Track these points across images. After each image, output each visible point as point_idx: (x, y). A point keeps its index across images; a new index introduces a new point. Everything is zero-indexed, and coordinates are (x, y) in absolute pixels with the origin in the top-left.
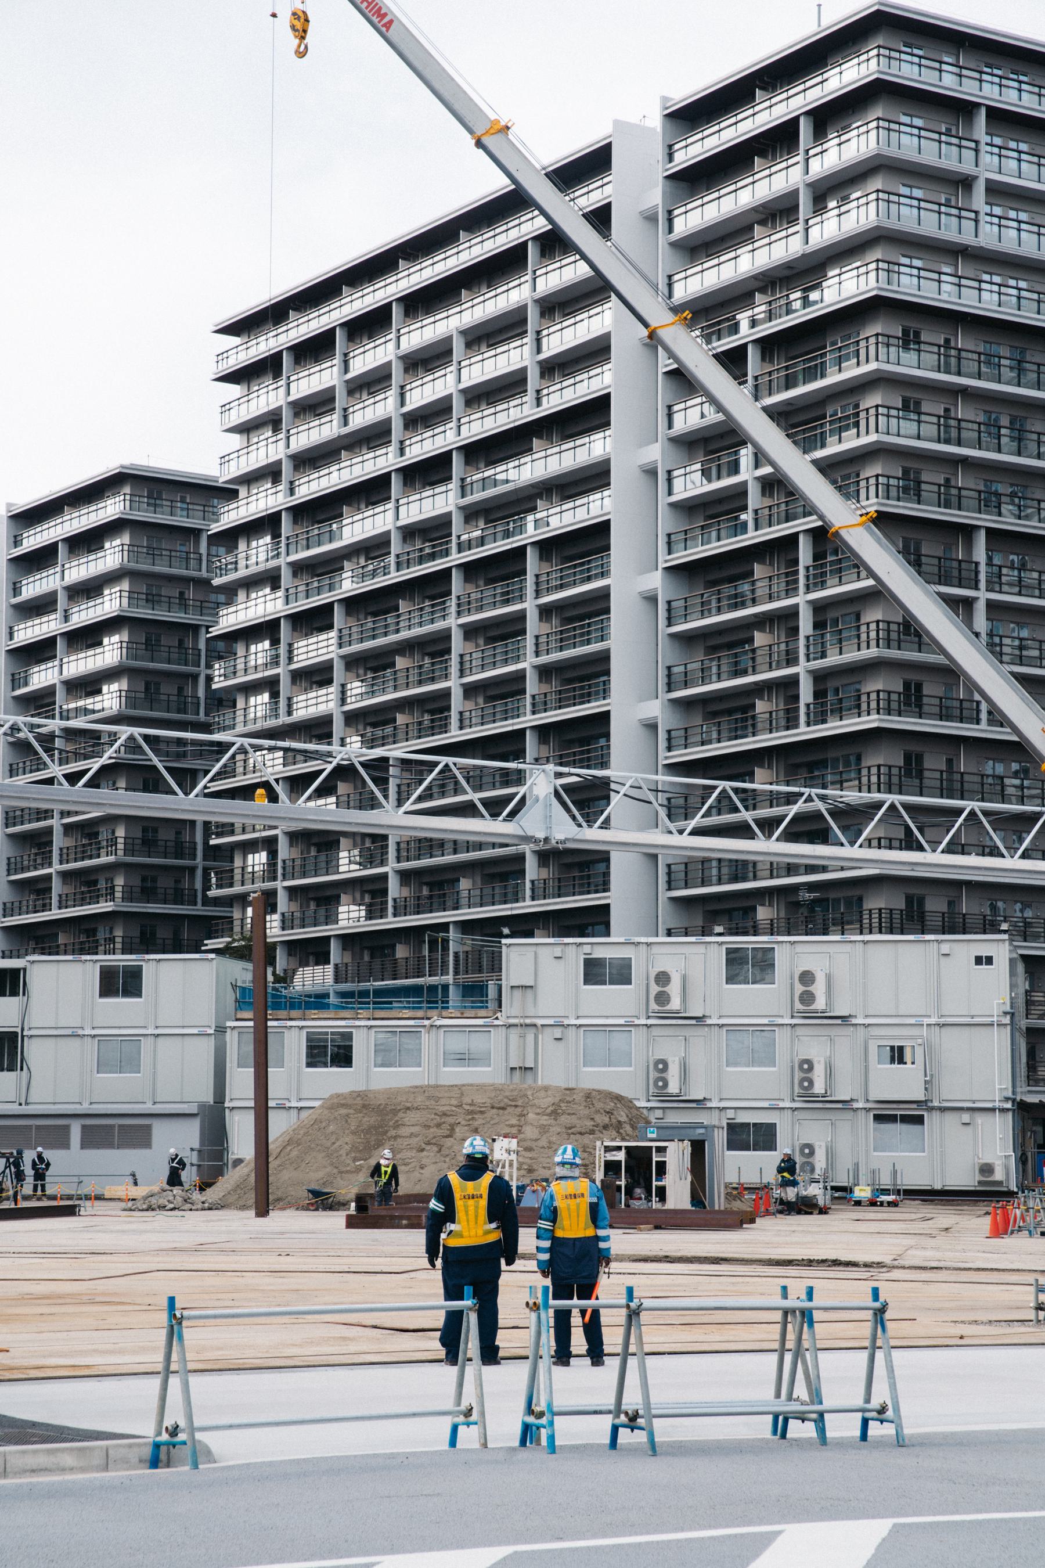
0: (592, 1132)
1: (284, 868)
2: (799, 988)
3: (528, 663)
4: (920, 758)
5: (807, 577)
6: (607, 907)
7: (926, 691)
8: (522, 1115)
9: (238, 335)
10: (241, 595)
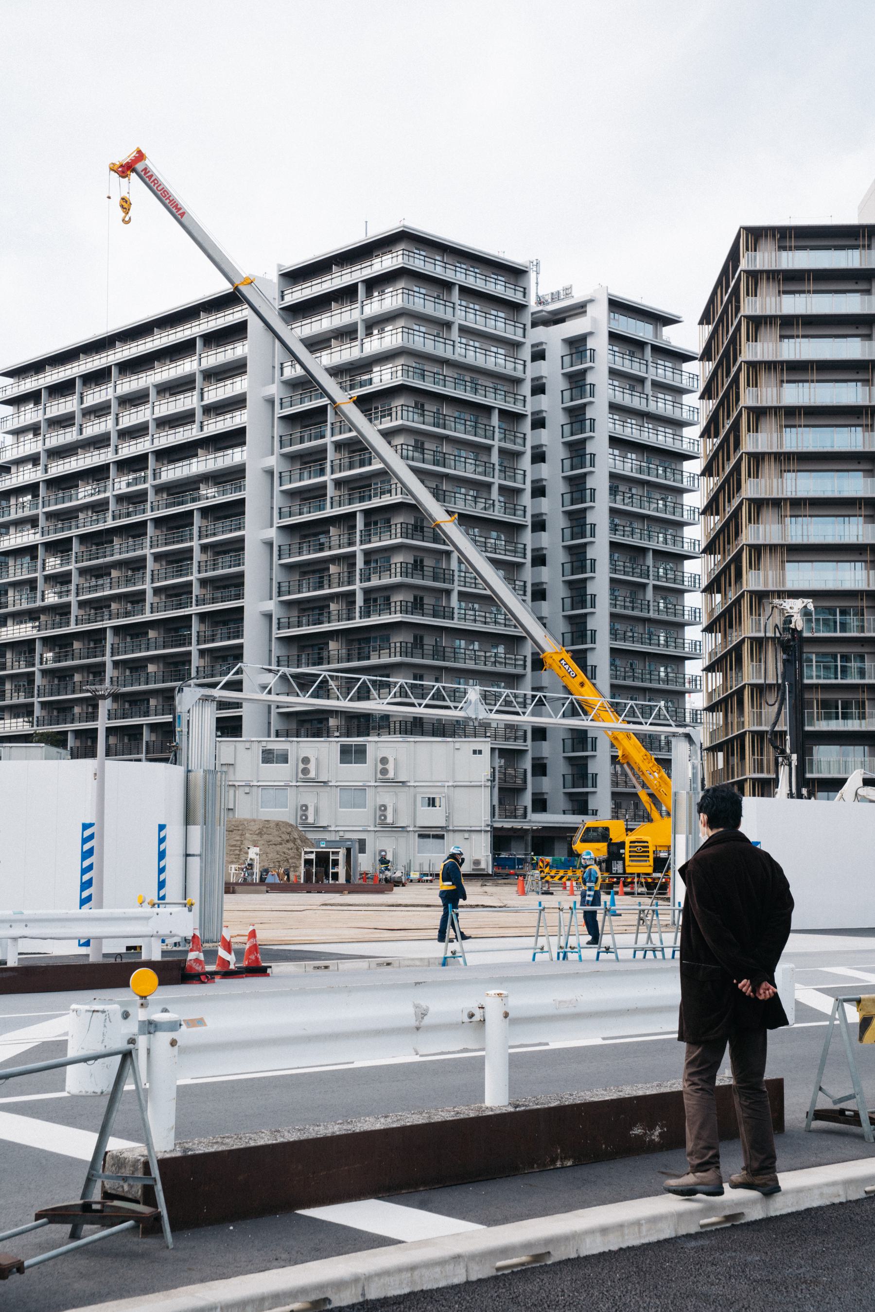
0: (281, 844)
1: (38, 691)
2: (380, 766)
3: (194, 577)
4: (422, 638)
5: (361, 536)
6: (241, 717)
7: (425, 602)
8: (242, 835)
9: (12, 377)
10: (12, 530)
